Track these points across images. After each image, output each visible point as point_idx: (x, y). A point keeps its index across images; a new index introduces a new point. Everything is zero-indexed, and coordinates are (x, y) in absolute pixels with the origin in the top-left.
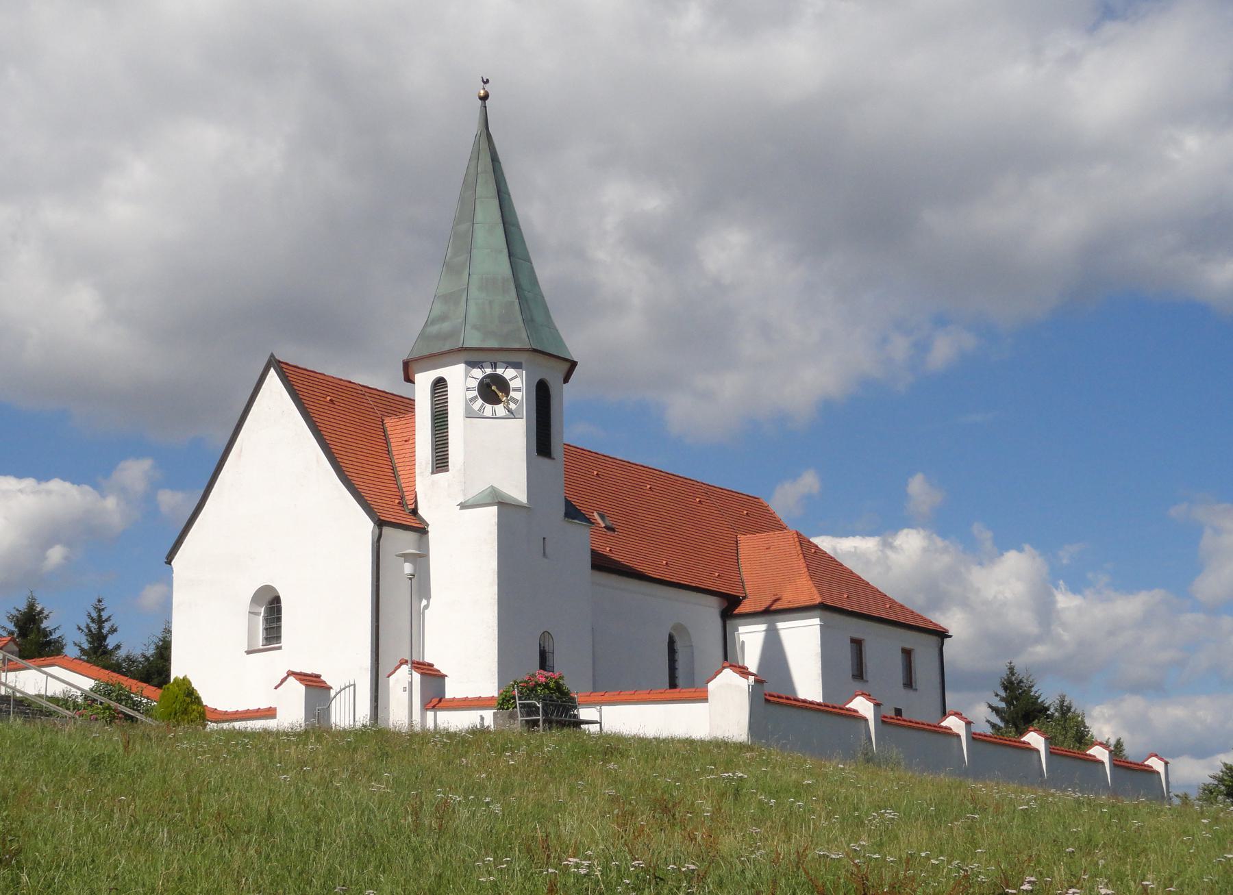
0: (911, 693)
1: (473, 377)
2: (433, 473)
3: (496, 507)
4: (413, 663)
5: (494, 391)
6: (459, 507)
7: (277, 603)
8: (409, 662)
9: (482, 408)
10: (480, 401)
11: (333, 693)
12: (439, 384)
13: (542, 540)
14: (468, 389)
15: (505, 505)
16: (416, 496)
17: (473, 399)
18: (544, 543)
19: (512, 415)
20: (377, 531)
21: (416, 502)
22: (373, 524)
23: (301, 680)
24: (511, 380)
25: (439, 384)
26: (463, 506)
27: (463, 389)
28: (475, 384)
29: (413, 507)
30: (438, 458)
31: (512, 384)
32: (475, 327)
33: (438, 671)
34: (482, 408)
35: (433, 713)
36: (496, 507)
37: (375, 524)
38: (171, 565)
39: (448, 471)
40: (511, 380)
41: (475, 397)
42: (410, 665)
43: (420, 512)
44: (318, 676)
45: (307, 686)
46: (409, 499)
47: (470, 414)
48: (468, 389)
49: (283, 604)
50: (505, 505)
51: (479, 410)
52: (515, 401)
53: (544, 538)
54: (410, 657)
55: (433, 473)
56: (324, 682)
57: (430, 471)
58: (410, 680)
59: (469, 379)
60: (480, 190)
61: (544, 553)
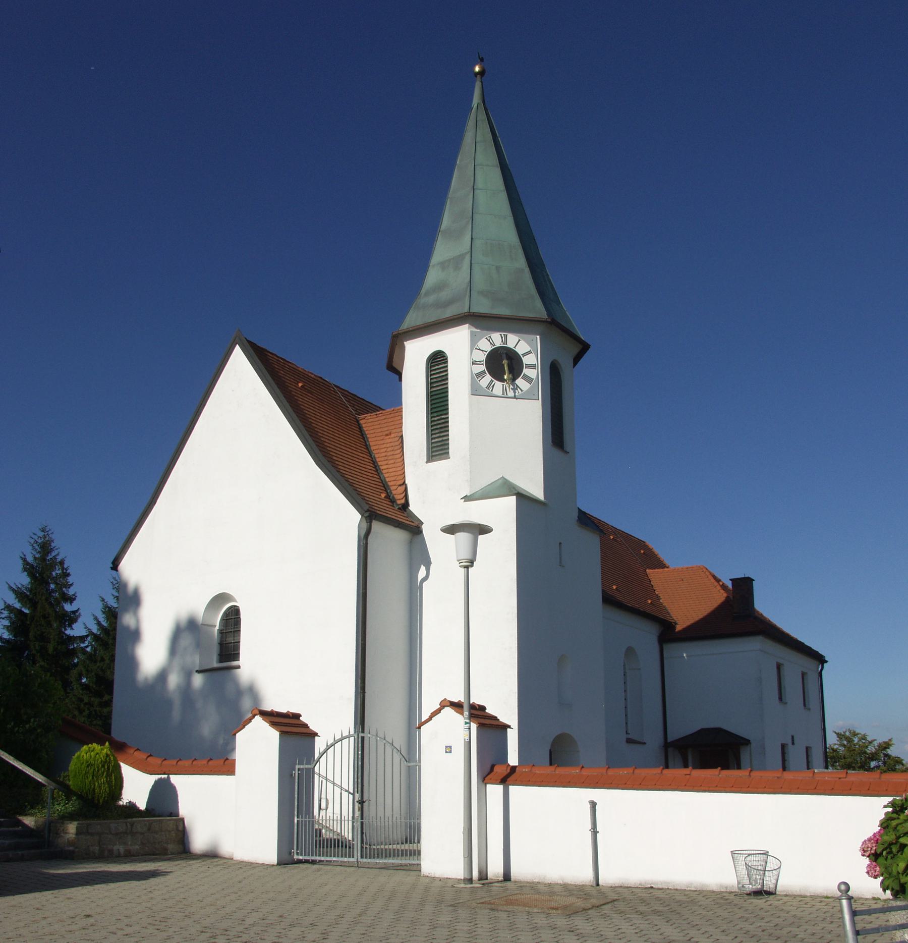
0: (73, 631)
1: (482, 351)
2: (428, 461)
3: (515, 497)
4: (473, 707)
5: (503, 365)
6: (463, 500)
7: (237, 615)
8: (466, 707)
9: (490, 386)
10: (488, 378)
11: (320, 744)
12: (437, 361)
13: (558, 544)
14: (475, 362)
15: (523, 499)
16: (406, 490)
17: (481, 375)
18: (560, 549)
19: (525, 397)
20: (365, 525)
21: (406, 497)
22: (360, 516)
23: (273, 724)
24: (524, 355)
25: (437, 361)
26: (467, 498)
27: (467, 363)
28: (482, 357)
29: (403, 501)
30: (433, 445)
31: (526, 360)
32: (482, 293)
33: (495, 718)
34: (490, 386)
35: (501, 786)
36: (515, 497)
37: (362, 515)
38: (117, 571)
39: (449, 458)
40: (524, 355)
41: (483, 372)
42: (466, 713)
43: (412, 508)
44: (297, 716)
45: (283, 734)
46: (397, 493)
47: (476, 391)
48: (474, 363)
49: (242, 616)
50: (523, 499)
51: (488, 387)
52: (528, 379)
53: (560, 543)
54: (467, 699)
55: (428, 461)
56: (305, 726)
57: (426, 460)
58: (467, 738)
59: (475, 351)
60: (480, 158)
61: (560, 562)
